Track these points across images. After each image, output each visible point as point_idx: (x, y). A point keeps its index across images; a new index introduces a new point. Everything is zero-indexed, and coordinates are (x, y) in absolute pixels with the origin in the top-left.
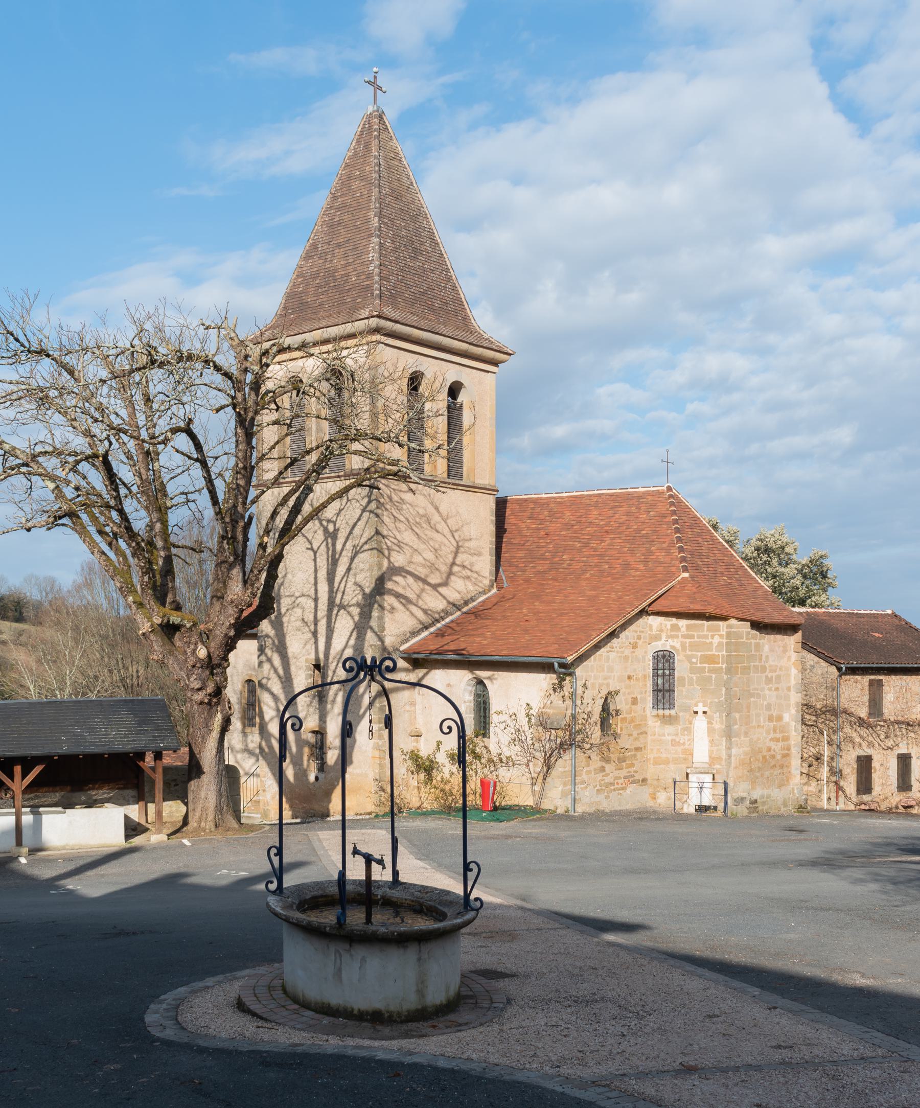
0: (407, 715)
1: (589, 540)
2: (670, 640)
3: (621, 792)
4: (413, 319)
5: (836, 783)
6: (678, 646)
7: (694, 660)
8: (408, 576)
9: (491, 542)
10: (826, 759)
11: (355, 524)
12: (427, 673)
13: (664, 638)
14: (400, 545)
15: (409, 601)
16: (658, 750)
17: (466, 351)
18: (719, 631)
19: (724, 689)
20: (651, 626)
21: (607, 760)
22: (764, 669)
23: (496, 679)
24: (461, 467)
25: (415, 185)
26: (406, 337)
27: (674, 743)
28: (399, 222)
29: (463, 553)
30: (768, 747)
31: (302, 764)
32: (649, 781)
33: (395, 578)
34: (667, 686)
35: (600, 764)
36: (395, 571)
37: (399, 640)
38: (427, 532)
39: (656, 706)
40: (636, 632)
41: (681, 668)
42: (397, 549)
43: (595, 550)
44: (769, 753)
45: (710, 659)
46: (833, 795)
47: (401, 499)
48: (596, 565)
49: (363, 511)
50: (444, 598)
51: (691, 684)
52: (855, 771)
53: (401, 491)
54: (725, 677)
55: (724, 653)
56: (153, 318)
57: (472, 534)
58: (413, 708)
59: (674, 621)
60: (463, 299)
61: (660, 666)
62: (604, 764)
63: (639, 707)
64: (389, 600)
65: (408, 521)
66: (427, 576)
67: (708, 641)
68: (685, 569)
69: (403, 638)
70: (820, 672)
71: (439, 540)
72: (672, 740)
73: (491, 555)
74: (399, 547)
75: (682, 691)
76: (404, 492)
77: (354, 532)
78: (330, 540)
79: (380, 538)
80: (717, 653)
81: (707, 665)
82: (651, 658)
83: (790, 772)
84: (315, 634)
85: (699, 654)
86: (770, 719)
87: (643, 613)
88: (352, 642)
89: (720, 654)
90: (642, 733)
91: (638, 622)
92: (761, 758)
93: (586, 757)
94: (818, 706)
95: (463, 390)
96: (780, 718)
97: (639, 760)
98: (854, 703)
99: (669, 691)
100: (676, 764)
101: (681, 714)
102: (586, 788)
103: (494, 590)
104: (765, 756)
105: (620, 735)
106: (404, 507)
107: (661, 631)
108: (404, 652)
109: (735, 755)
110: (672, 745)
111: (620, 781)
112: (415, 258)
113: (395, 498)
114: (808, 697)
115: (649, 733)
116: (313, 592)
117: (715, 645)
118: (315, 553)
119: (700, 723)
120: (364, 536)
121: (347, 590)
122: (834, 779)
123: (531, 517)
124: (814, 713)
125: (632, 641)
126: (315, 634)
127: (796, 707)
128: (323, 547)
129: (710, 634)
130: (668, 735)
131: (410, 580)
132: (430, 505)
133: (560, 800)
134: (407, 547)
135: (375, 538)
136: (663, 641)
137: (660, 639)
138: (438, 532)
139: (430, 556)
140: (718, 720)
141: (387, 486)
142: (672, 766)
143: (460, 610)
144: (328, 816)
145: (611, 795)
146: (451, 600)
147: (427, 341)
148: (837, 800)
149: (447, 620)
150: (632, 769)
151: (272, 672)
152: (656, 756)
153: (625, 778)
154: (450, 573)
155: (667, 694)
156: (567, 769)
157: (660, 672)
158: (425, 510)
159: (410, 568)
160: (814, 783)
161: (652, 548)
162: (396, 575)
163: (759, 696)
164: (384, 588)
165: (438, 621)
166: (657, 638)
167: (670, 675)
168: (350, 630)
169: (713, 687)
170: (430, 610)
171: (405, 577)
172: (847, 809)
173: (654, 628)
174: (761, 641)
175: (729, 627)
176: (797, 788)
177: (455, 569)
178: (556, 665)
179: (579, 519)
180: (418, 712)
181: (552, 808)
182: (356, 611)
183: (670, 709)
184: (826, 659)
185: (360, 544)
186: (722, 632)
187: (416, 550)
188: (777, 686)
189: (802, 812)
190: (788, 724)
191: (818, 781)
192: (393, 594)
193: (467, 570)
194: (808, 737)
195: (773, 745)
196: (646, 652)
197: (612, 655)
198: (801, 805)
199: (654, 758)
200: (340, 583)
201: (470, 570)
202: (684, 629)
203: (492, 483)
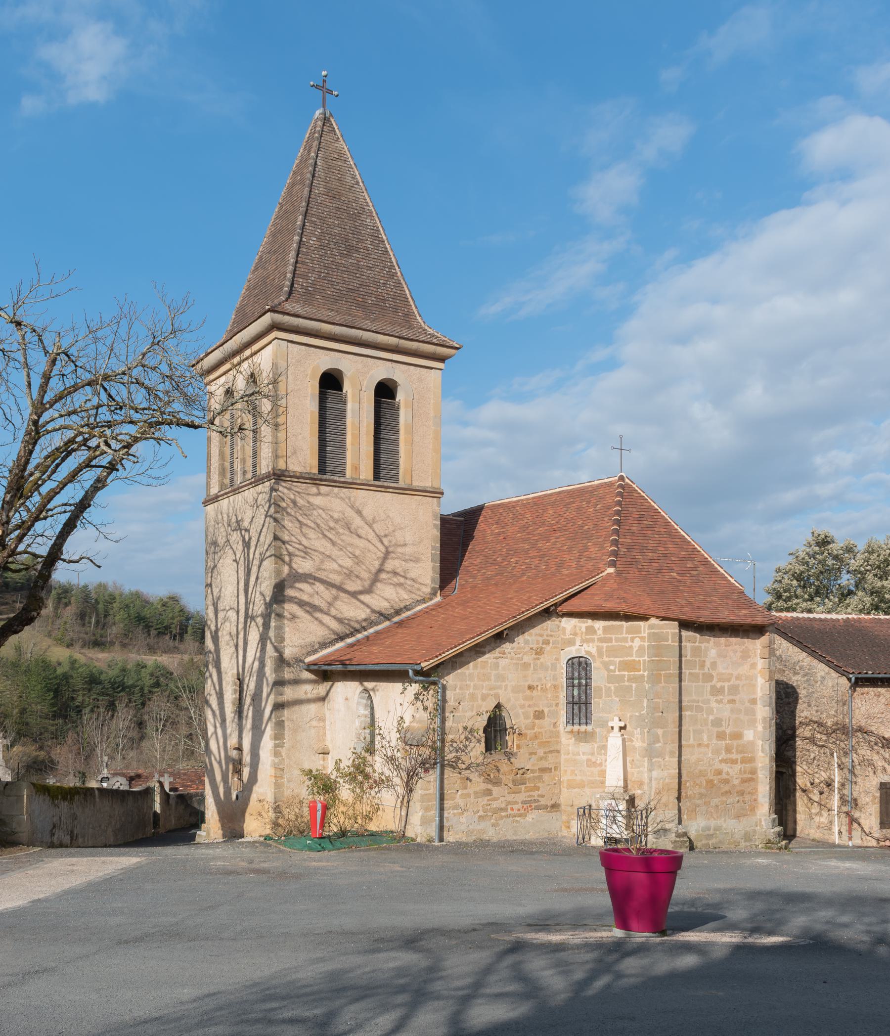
1: (537, 540)
2: (585, 645)
4: (325, 314)
5: (847, 813)
6: (594, 651)
7: (612, 667)
8: (317, 584)
9: (434, 548)
10: (836, 785)
12: (331, 687)
13: (578, 643)
14: (306, 552)
16: (573, 772)
17: (397, 346)
18: (640, 632)
19: (646, 700)
20: (564, 629)
21: (497, 783)
22: (709, 677)
24: (397, 469)
25: (361, 184)
27: (590, 764)
28: (332, 221)
29: (393, 559)
30: (716, 770)
31: (228, 783)
32: (563, 807)
33: (297, 585)
34: (583, 698)
35: (484, 786)
36: (298, 577)
37: (304, 651)
38: (343, 537)
39: (571, 721)
40: (541, 636)
41: (598, 678)
42: (302, 554)
44: (719, 777)
45: (630, 666)
46: (844, 829)
47: (309, 502)
49: (266, 516)
50: (368, 606)
51: (609, 695)
52: (878, 800)
53: (308, 494)
54: (647, 686)
55: (646, 658)
56: (99, 345)
57: (407, 539)
58: (322, 724)
59: (589, 622)
61: (576, 674)
62: (490, 786)
63: (547, 722)
64: (289, 608)
65: (318, 526)
66: (342, 583)
67: (627, 645)
68: (613, 564)
69: (309, 649)
70: (830, 684)
71: (362, 545)
72: (588, 760)
73: (433, 560)
74: (305, 553)
75: (599, 704)
76: (313, 495)
79: (279, 543)
80: (637, 659)
81: (626, 673)
82: (564, 666)
83: (755, 800)
84: (237, 646)
85: (618, 660)
86: (721, 736)
87: (547, 613)
88: (258, 654)
89: (641, 659)
90: (551, 752)
91: (545, 624)
92: (704, 783)
94: (829, 724)
95: (399, 388)
96: (738, 736)
98: (875, 720)
99: (573, 703)
100: (592, 788)
101: (598, 730)
102: (462, 813)
103: (438, 599)
104: (712, 781)
105: (516, 753)
106: (315, 512)
107: (575, 634)
108: (309, 665)
109: (656, 779)
110: (588, 766)
111: (516, 807)
112: (349, 255)
113: (301, 502)
114: (819, 713)
115: (562, 752)
117: (635, 649)
118: (238, 564)
119: (615, 741)
122: (845, 809)
123: (497, 523)
124: (825, 732)
125: (535, 646)
126: (237, 646)
127: (763, 723)
129: (630, 636)
130: (584, 753)
134: (316, 553)
136: (577, 647)
137: (574, 644)
138: (359, 537)
140: (639, 736)
141: (289, 489)
142: (587, 790)
143: (389, 620)
144: (242, 836)
145: (500, 822)
146: (377, 609)
147: (343, 336)
148: (850, 833)
149: (371, 631)
150: (536, 793)
152: (570, 778)
153: (524, 802)
154: (375, 580)
155: (583, 707)
156: (431, 791)
157: (576, 682)
158: (344, 515)
159: (322, 575)
160: (825, 813)
161: (589, 544)
162: (299, 581)
163: (699, 709)
165: (358, 631)
166: (571, 643)
167: (586, 685)
169: (633, 698)
172: (865, 844)
173: (568, 632)
174: (703, 646)
175: (651, 627)
176: (765, 820)
177: (383, 576)
178: (411, 673)
179: (536, 519)
180: (327, 727)
181: (414, 836)
182: (260, 621)
183: (587, 724)
184: (836, 668)
186: (643, 635)
188: (731, 697)
189: (770, 848)
190: (752, 743)
191: (829, 810)
192: (296, 603)
194: (819, 760)
195: (725, 768)
196: (557, 659)
197: (503, 662)
198: (769, 840)
199: (568, 780)
202: (600, 632)
203: (436, 485)
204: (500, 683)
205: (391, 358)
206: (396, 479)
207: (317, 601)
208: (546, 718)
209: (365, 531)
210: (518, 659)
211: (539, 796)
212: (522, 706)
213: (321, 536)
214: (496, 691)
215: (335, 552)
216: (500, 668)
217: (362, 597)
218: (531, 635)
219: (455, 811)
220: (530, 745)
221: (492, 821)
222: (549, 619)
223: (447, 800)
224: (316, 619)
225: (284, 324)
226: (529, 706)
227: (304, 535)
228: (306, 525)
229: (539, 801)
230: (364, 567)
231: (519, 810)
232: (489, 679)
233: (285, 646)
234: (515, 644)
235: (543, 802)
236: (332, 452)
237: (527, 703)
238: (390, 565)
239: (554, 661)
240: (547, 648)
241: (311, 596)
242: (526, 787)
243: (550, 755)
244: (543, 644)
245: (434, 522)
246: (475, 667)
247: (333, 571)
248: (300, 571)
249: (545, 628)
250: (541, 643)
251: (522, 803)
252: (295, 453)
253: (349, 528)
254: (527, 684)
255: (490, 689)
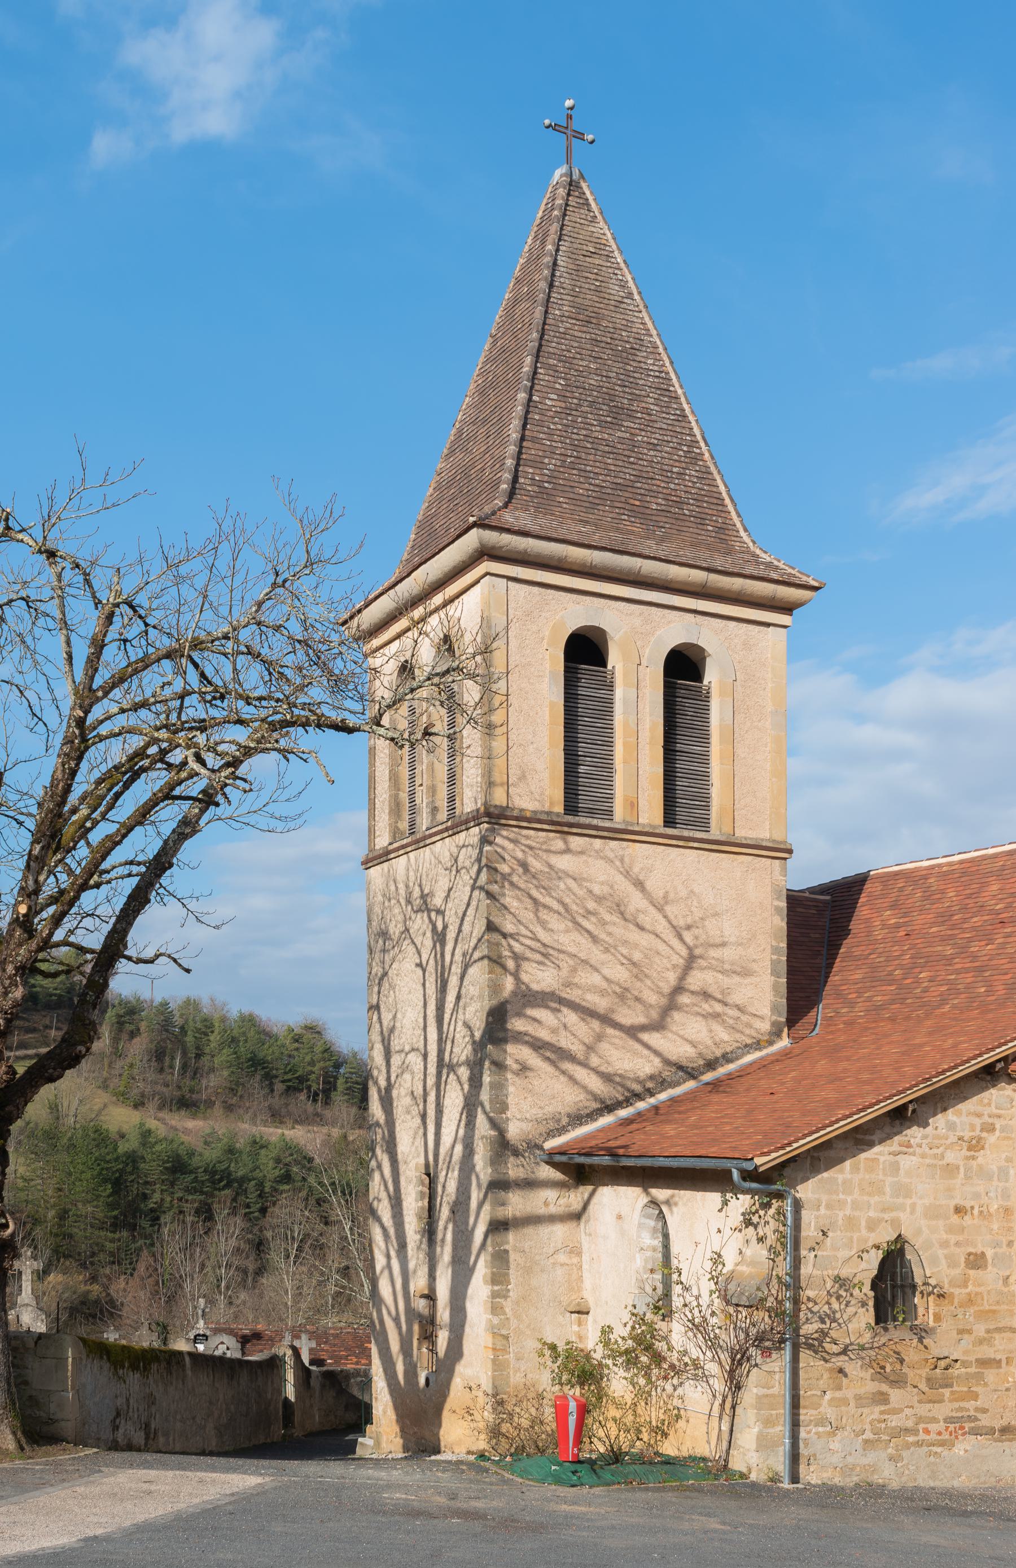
0: (560, 1272)
1: (970, 940)
3: (939, 1450)
4: (573, 529)
8: (565, 1010)
9: (775, 950)
11: (464, 914)
12: (592, 1194)
14: (546, 954)
15: (572, 1058)
17: (704, 586)
21: (898, 1381)
23: (676, 1204)
24: (707, 807)
25: (636, 297)
26: (554, 563)
28: (584, 363)
33: (530, 1012)
37: (542, 1129)
38: (610, 928)
40: (979, 1115)
42: (538, 957)
43: (974, 958)
47: (550, 866)
48: (968, 987)
49: (473, 888)
50: (657, 1053)
57: (726, 933)
60: (725, 495)
62: (885, 1387)
64: (515, 1053)
65: (565, 905)
69: (552, 1125)
73: (774, 973)
77: (463, 928)
78: (438, 945)
79: (496, 937)
84: (424, 1116)
88: (461, 1132)
90: (999, 1330)
91: (986, 1095)
93: (831, 1370)
97: (992, 1387)
108: (551, 1153)
111: (933, 1427)
112: (616, 425)
113: (535, 864)
116: (422, 1042)
118: (424, 971)
120: (474, 935)
121: (457, 1036)
123: (894, 906)
125: (967, 1135)
126: (424, 1116)
128: (432, 962)
131: (571, 1017)
132: (620, 878)
133: (755, 1454)
134: (561, 956)
135: (486, 937)
139: (620, 974)
143: (694, 1078)
145: (905, 1454)
146: (673, 1058)
147: (605, 568)
149: (663, 1096)
150: (971, 1405)
151: (382, 1188)
153: (949, 1420)
156: (775, 1390)
158: (612, 887)
159: (568, 994)
162: (534, 1006)
164: (506, 1030)
165: (639, 1097)
168: (460, 1109)
170: (620, 1076)
171: (559, 1011)
177: (684, 999)
179: (967, 901)
181: (744, 1470)
182: (464, 1072)
185: (470, 951)
187: (585, 962)
192: (527, 1043)
193: (713, 1002)
197: (906, 1162)
200: (449, 1024)
201: (719, 1001)
203: (778, 836)
204: (901, 1200)
205: (694, 607)
206: (704, 824)
207: (564, 1041)
208: (990, 1268)
209: (651, 918)
210: (935, 1156)
211: (977, 1409)
212: (944, 1244)
213: (570, 924)
214: (893, 1214)
215: (596, 955)
216: (902, 1172)
217: (645, 1037)
218: (959, 1114)
219: (821, 1429)
220: (960, 1316)
221: (890, 1451)
222: (994, 1086)
223: (805, 1407)
224: (564, 1072)
225: (501, 547)
226: (957, 1244)
227: (543, 924)
228: (545, 906)
229: (976, 1419)
230: (648, 982)
231: (940, 1433)
232: (881, 1192)
233: (508, 1119)
234: (929, 1129)
235: (985, 1421)
236: (588, 775)
237: (953, 1239)
238: (696, 979)
239: (1003, 1163)
240: (991, 1139)
241: (554, 1031)
242: (952, 1393)
243: (997, 1336)
244: (982, 1130)
245: (776, 903)
246: (855, 1169)
247: (593, 989)
248: (535, 987)
249: (986, 1101)
250: (978, 1128)
251: (945, 1421)
252: (523, 777)
253: (622, 914)
254: (952, 1203)
255: (884, 1210)
